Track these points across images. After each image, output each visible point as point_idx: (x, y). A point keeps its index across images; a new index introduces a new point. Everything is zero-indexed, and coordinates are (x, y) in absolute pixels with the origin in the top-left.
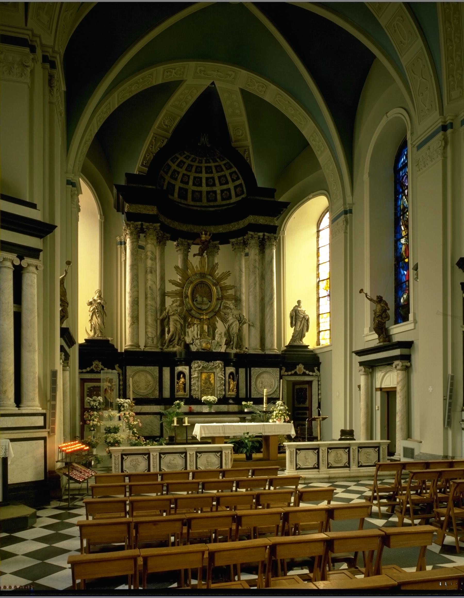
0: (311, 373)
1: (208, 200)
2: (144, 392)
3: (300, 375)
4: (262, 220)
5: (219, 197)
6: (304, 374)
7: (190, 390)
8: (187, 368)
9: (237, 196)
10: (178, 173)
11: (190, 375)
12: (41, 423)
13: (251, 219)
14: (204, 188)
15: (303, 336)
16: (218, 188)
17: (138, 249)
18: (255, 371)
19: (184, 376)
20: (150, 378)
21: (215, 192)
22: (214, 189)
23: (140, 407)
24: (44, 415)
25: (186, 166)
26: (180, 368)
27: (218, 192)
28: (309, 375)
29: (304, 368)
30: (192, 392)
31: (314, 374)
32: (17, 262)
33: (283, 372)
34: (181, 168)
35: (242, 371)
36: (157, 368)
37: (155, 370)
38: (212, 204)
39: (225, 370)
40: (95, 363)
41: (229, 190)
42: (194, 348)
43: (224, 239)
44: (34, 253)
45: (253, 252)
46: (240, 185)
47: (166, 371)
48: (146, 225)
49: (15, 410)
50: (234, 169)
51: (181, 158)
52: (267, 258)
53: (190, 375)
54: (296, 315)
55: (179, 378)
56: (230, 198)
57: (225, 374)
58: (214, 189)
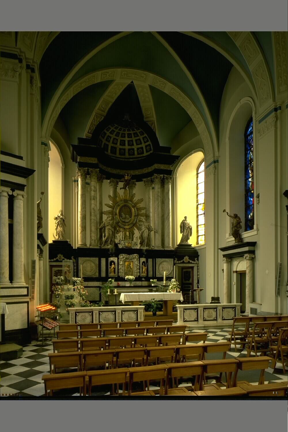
0: (193, 262)
1: (129, 154)
2: (89, 274)
3: (186, 263)
4: (162, 167)
5: (136, 153)
6: (189, 262)
7: (118, 272)
8: (116, 258)
9: (147, 152)
10: (114, 131)
11: (118, 263)
12: (26, 293)
13: (156, 166)
14: (127, 147)
15: (188, 239)
16: (135, 147)
17: (85, 185)
18: (158, 260)
19: (114, 264)
20: (93, 265)
21: (133, 149)
22: (133, 147)
23: (87, 283)
24: (27, 288)
25: (115, 133)
26: (111, 259)
27: (136, 149)
28: (192, 263)
29: (189, 259)
30: (119, 274)
31: (195, 262)
32: (11, 193)
33: (176, 261)
34: (113, 134)
35: (150, 261)
36: (97, 259)
37: (96, 260)
38: (131, 157)
39: (139, 260)
40: (59, 256)
41: (142, 148)
42: (120, 246)
43: (139, 178)
44: (21, 187)
45: (157, 186)
46: (149, 145)
47: (103, 261)
48: (90, 169)
49: (10, 285)
50: (145, 135)
51: (112, 128)
52: (166, 191)
53: (118, 263)
54: (184, 226)
55: (111, 265)
56: (143, 153)
57: (139, 262)
58: (133, 147)
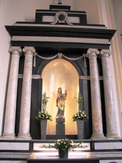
32: (98, 53)
49: (104, 138)
